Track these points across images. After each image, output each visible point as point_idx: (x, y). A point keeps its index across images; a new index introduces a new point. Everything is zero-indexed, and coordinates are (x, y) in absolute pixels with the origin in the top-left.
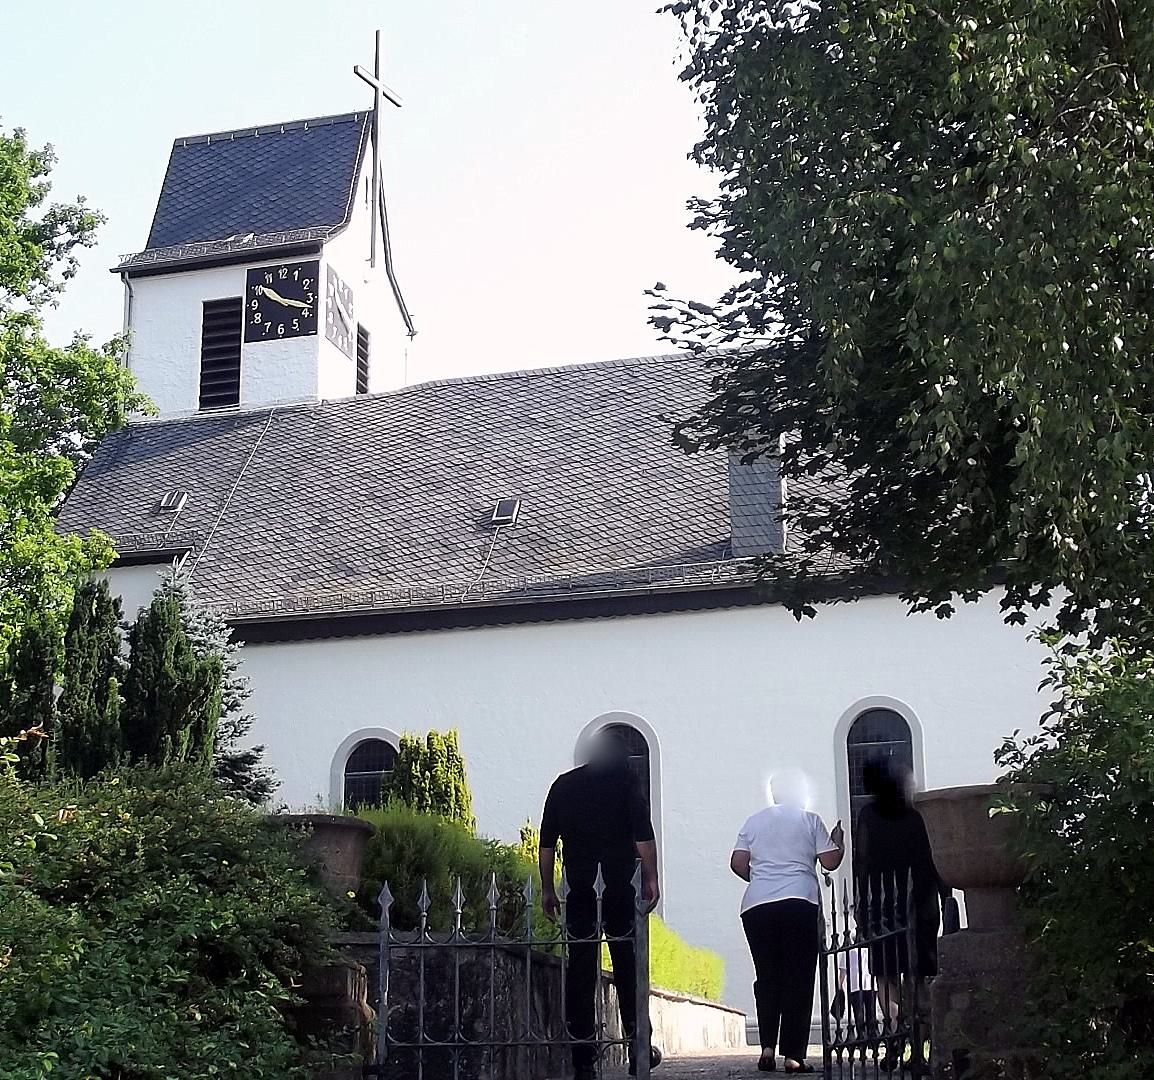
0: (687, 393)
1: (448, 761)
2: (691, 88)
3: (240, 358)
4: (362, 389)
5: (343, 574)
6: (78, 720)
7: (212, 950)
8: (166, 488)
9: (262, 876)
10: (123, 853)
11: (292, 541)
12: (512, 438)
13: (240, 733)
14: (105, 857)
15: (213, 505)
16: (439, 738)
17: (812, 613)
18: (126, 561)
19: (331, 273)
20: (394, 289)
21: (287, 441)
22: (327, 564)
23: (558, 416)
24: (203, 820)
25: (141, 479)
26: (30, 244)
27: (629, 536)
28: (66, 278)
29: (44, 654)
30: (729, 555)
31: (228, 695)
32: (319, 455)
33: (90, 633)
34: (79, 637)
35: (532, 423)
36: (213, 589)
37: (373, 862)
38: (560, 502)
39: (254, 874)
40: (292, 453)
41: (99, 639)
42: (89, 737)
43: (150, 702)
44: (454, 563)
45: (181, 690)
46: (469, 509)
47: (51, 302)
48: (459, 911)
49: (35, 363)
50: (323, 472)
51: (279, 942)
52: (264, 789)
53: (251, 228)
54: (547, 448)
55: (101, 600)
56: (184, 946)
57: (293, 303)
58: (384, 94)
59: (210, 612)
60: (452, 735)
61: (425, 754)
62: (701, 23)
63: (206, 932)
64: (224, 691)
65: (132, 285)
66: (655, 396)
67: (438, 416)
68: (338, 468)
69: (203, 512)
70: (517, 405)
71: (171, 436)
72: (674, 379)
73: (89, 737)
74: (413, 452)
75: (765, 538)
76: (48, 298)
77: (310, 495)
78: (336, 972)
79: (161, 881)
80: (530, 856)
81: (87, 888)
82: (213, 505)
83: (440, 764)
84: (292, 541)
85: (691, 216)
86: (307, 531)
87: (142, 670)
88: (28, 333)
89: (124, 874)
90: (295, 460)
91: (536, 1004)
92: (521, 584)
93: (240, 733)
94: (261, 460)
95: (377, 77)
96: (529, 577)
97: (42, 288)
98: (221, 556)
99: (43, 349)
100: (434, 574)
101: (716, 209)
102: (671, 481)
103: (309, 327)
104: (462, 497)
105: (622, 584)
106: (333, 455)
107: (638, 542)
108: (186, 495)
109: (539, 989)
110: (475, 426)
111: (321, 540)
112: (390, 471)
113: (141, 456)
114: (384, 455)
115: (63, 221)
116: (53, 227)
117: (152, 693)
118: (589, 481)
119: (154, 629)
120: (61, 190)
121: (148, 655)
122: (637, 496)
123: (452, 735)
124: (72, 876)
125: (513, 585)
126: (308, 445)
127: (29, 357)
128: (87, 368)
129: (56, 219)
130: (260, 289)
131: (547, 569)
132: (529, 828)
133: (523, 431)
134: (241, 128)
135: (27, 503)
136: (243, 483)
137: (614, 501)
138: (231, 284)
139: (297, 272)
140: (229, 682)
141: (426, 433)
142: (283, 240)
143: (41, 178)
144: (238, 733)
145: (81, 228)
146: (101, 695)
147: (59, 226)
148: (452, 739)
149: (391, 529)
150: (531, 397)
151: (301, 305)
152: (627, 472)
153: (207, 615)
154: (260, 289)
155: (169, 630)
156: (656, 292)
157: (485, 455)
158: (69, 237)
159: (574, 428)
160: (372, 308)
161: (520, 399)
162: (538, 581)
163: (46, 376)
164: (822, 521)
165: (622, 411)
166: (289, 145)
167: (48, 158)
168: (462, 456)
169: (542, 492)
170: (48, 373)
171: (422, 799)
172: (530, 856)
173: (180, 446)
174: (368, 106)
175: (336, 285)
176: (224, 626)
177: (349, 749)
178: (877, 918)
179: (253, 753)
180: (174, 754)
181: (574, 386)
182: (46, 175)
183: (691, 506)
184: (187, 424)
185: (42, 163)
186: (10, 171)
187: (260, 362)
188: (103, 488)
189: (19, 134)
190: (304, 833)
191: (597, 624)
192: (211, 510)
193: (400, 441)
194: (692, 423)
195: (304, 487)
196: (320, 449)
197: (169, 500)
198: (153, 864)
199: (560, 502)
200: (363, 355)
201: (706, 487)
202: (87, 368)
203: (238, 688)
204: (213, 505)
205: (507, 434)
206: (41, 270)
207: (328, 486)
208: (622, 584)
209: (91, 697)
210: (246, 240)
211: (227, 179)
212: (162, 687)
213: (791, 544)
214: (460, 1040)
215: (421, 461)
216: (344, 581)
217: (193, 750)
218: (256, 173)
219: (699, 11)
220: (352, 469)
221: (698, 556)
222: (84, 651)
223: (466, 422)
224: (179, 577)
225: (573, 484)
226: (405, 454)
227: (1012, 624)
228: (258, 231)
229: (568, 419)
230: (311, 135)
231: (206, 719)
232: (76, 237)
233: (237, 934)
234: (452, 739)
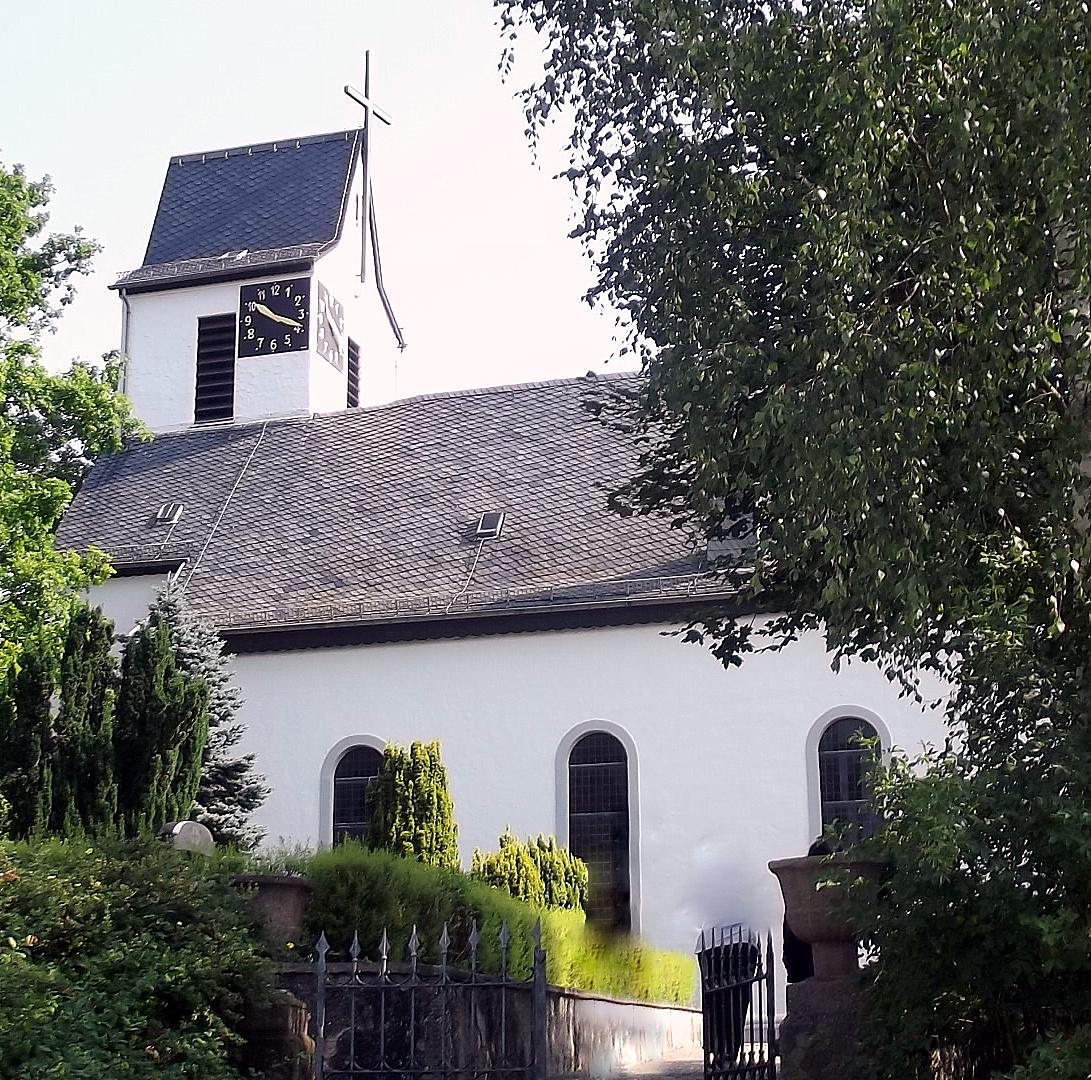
1: (431, 771)
2: (582, 242)
3: (233, 385)
4: (352, 402)
5: (332, 586)
6: (74, 740)
7: (168, 998)
8: (163, 500)
9: (211, 933)
12: (497, 452)
13: (232, 741)
14: (78, 920)
15: (208, 517)
16: (423, 748)
17: (738, 662)
18: (125, 572)
19: (321, 289)
20: (384, 303)
21: (279, 454)
22: (318, 576)
23: (542, 430)
24: (162, 888)
25: (139, 492)
26: (29, 273)
27: (609, 549)
28: (64, 304)
29: (40, 679)
31: (220, 705)
32: (311, 467)
35: (518, 437)
37: (328, 898)
38: (542, 515)
39: (205, 932)
40: (284, 466)
41: (93, 663)
42: (84, 756)
43: (141, 723)
45: (171, 711)
48: (385, 957)
49: (34, 391)
50: (314, 484)
51: (224, 990)
52: (255, 796)
53: (244, 245)
54: (530, 462)
55: (95, 625)
56: (145, 995)
59: (203, 625)
60: (435, 745)
61: (409, 764)
62: (592, 189)
63: (162, 983)
64: (217, 701)
65: (129, 302)
67: (425, 430)
68: (328, 480)
70: (503, 419)
71: (169, 447)
73: (84, 756)
74: (401, 465)
78: (279, 1011)
79: (125, 938)
80: (508, 863)
81: (63, 946)
82: (207, 517)
83: (422, 774)
86: (298, 542)
87: (134, 693)
88: (27, 361)
89: (94, 934)
91: (479, 1023)
92: (504, 595)
93: (232, 741)
94: (254, 473)
95: (367, 96)
97: (40, 314)
98: (215, 567)
99: (41, 377)
100: (420, 586)
103: (300, 342)
104: (448, 510)
106: (324, 468)
108: (181, 507)
109: (481, 1010)
110: (461, 439)
111: (311, 552)
112: (378, 484)
113: (138, 470)
114: (373, 468)
115: (61, 250)
116: (51, 256)
117: (143, 715)
118: (571, 494)
119: (142, 653)
120: (59, 220)
121: (140, 679)
123: (435, 745)
124: (51, 936)
125: (496, 597)
126: (300, 458)
128: (84, 395)
129: (54, 248)
130: (253, 306)
131: (529, 581)
132: (508, 835)
134: (236, 146)
138: (224, 301)
139: (288, 289)
140: (222, 693)
141: (413, 447)
142: (276, 257)
143: (40, 209)
144: (229, 742)
145: (78, 257)
146: (95, 718)
147: (57, 254)
148: (435, 749)
150: (516, 411)
151: (292, 322)
153: (200, 628)
154: (253, 306)
155: (158, 655)
157: (471, 469)
158: (66, 265)
159: (557, 442)
160: (362, 322)
161: (506, 414)
162: (520, 593)
166: (281, 163)
167: (46, 188)
168: (448, 470)
169: (525, 505)
170: (46, 400)
171: (405, 807)
172: (508, 863)
174: (359, 125)
175: (327, 301)
176: (217, 639)
177: (335, 759)
178: (735, 965)
179: (245, 762)
180: (164, 772)
181: (558, 400)
184: (183, 437)
185: (40, 193)
186: (9, 206)
187: (253, 376)
188: (101, 500)
189: (17, 170)
190: (251, 893)
191: (577, 635)
193: (388, 455)
194: (625, 491)
195: (295, 499)
196: (311, 462)
198: (119, 922)
199: (542, 515)
200: (353, 368)
202: (84, 395)
203: (230, 699)
204: (208, 517)
205: (491, 448)
207: (318, 498)
209: (85, 718)
211: (221, 197)
212: (153, 709)
214: (385, 1068)
215: (408, 474)
216: (333, 592)
217: (182, 768)
218: (248, 191)
219: (590, 177)
222: (78, 675)
223: (452, 436)
224: (173, 592)
226: (394, 467)
227: (927, 669)
229: (551, 433)
230: (303, 153)
231: (194, 739)
232: (73, 265)
233: (188, 985)
234: (435, 749)
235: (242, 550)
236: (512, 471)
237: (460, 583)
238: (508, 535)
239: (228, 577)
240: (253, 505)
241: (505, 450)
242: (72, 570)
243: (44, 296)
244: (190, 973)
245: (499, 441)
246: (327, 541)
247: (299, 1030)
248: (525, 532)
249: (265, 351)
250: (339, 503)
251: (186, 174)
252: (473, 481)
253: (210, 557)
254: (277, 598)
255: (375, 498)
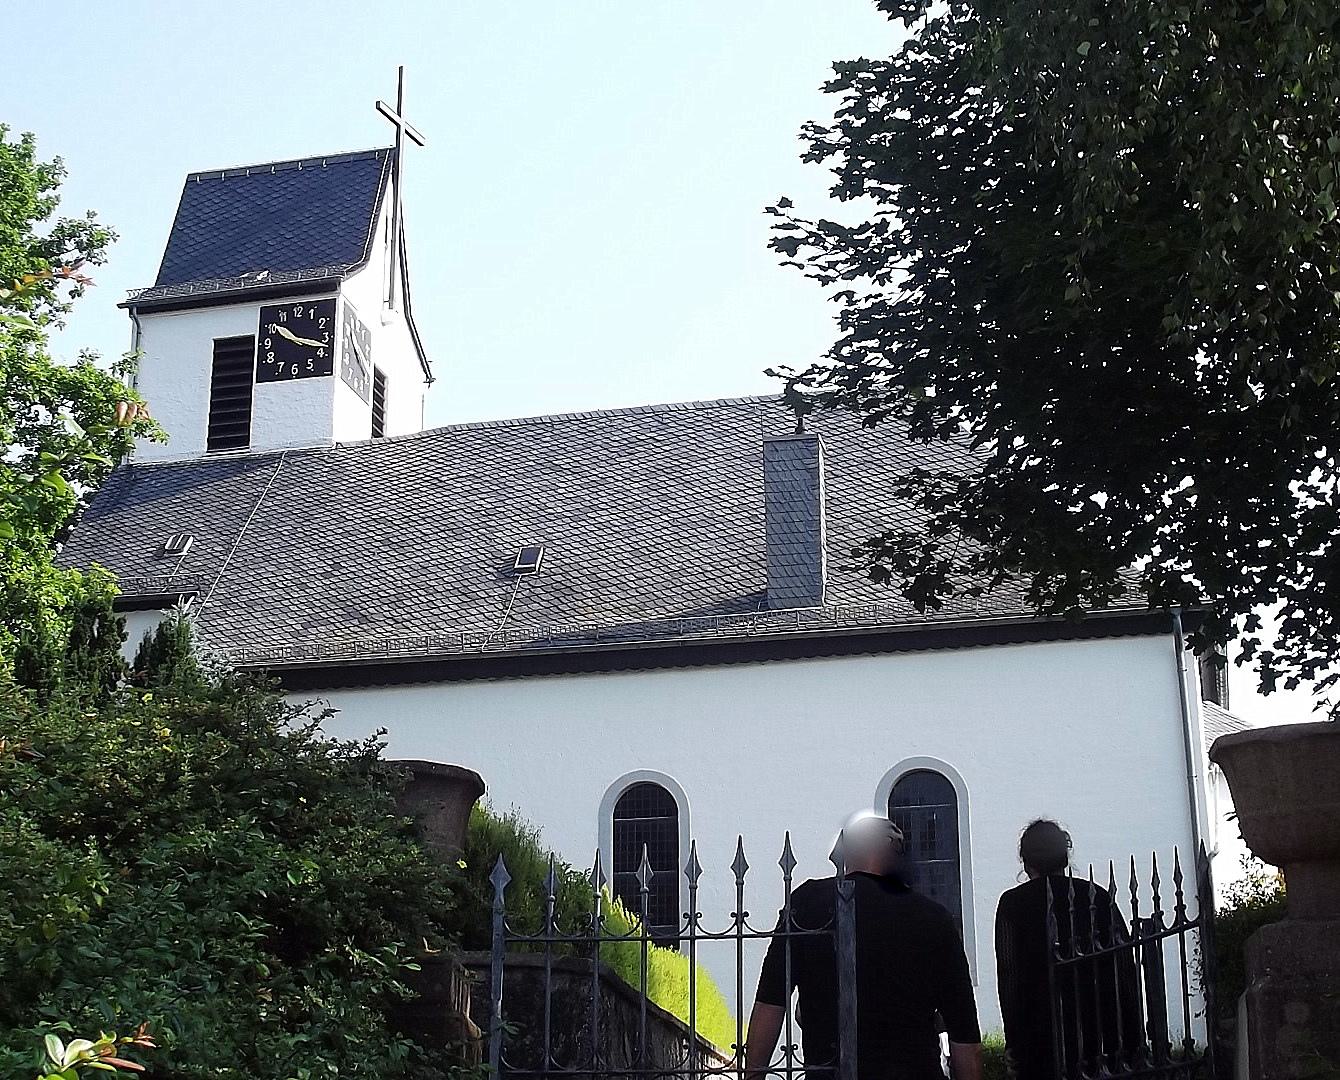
0: (719, 441)
4: (376, 434)
5: (356, 622)
10: (161, 778)
11: (303, 586)
19: (349, 313)
22: (340, 612)
30: (766, 607)
32: (333, 499)
33: (91, 654)
34: (79, 658)
36: (218, 635)
38: (585, 550)
44: (474, 612)
46: (490, 556)
47: (56, 323)
49: (38, 380)
54: (572, 495)
57: (307, 341)
58: (406, 132)
66: (685, 444)
69: (210, 556)
71: (176, 478)
72: (706, 427)
75: (803, 589)
76: (53, 318)
77: (323, 540)
82: (220, 549)
84: (303, 586)
85: (805, 146)
89: (161, 808)
90: (307, 504)
96: (554, 628)
101: (835, 137)
102: (703, 530)
103: (324, 367)
104: (483, 544)
105: (653, 635)
107: (668, 592)
108: (191, 538)
111: (333, 586)
113: (145, 499)
115: (71, 236)
116: (61, 242)
118: (616, 529)
122: (667, 545)
124: (86, 807)
125: (536, 635)
127: (32, 373)
128: (93, 387)
129: (65, 233)
133: (547, 477)
135: (24, 533)
136: (252, 527)
137: (644, 551)
138: (243, 322)
142: (300, 277)
143: (49, 192)
145: (91, 245)
149: (407, 576)
152: (657, 520)
153: (213, 657)
155: (178, 653)
156: (781, 210)
157: (507, 502)
158: (76, 254)
159: (600, 475)
160: (390, 351)
162: (563, 631)
163: (49, 395)
164: (949, 499)
165: (651, 458)
167: (57, 171)
168: (482, 502)
169: (568, 541)
170: (51, 392)
173: (186, 488)
182: (54, 189)
183: (724, 556)
184: (200, 464)
185: (50, 177)
186: (16, 177)
192: (218, 554)
196: (333, 494)
197: (175, 541)
198: (200, 792)
199: (585, 550)
201: (740, 537)
205: (529, 480)
206: (46, 289)
207: (341, 531)
208: (653, 635)
210: (259, 278)
211: (241, 216)
213: (830, 596)
215: (439, 506)
220: (367, 514)
221: (732, 607)
222: (83, 673)
225: (600, 533)
226: (424, 499)
228: (273, 269)
229: (594, 466)
230: (330, 172)
233: (319, 898)
235: (257, 583)
236: (552, 505)
237: (496, 620)
238: (548, 571)
239: (242, 612)
240: (270, 537)
241: (545, 483)
242: (73, 589)
243: (51, 288)
244: (323, 879)
245: (538, 473)
246: (350, 575)
247: (462, 1007)
248: (567, 568)
249: (286, 375)
250: (364, 536)
251: (202, 190)
252: (509, 514)
253: (223, 591)
254: (296, 634)
255: (404, 531)
